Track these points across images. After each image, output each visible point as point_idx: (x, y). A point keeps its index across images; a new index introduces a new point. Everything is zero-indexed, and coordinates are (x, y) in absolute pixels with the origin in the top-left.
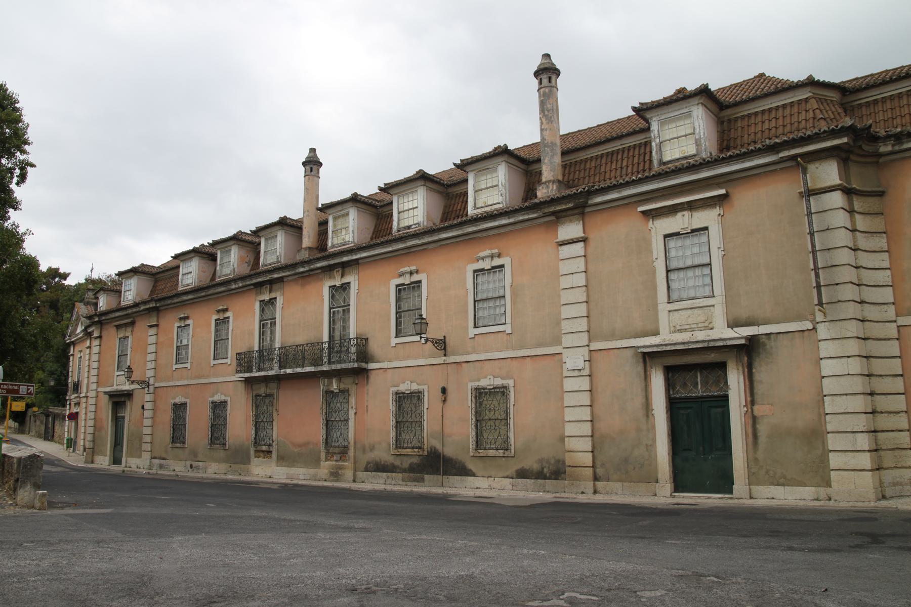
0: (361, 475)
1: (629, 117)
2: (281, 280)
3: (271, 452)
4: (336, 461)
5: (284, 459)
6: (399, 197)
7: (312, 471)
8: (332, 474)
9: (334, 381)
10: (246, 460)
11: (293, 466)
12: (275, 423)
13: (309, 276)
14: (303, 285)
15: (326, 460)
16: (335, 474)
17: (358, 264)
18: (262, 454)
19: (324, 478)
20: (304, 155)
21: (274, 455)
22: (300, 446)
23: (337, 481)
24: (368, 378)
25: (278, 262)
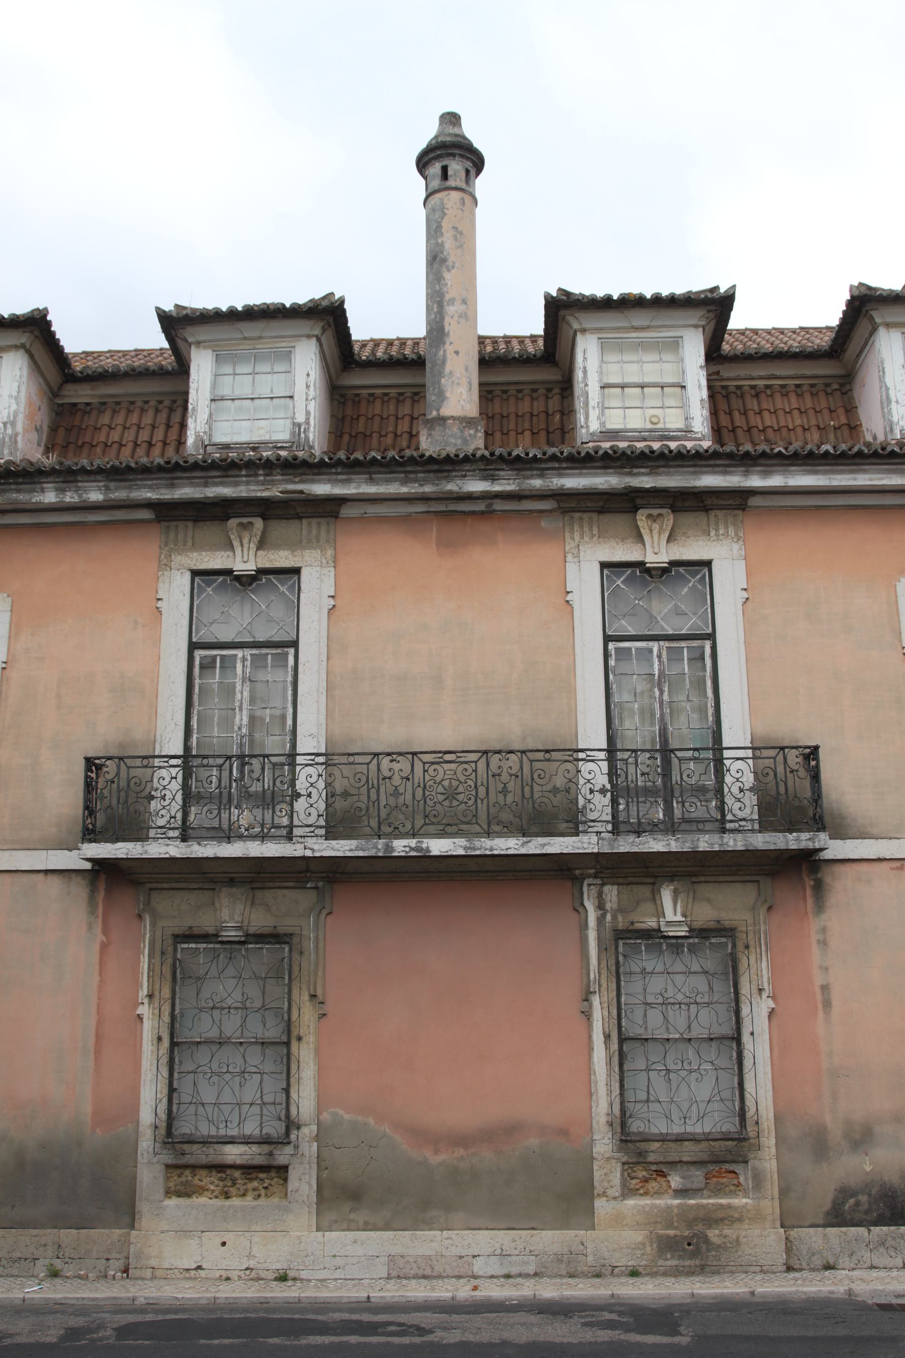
0: (816, 1239)
1: (161, 349)
2: (329, 509)
3: (283, 1170)
4: (681, 1193)
5: (346, 1197)
6: (219, 360)
7: (549, 1240)
8: (667, 1246)
9: (666, 896)
10: (119, 1206)
11: (429, 1225)
12: (306, 1056)
13: (487, 514)
14: (446, 545)
15: (627, 1192)
16: (689, 1246)
17: (743, 507)
18: (210, 1181)
19: (624, 1261)
20: (427, 132)
21: (303, 1181)
22: (460, 1140)
23: (702, 1270)
24: (819, 888)
25: (291, 445)
